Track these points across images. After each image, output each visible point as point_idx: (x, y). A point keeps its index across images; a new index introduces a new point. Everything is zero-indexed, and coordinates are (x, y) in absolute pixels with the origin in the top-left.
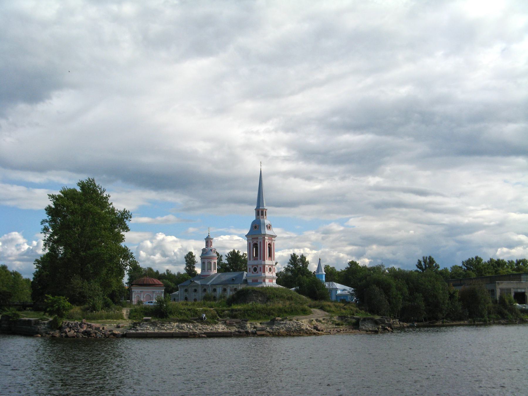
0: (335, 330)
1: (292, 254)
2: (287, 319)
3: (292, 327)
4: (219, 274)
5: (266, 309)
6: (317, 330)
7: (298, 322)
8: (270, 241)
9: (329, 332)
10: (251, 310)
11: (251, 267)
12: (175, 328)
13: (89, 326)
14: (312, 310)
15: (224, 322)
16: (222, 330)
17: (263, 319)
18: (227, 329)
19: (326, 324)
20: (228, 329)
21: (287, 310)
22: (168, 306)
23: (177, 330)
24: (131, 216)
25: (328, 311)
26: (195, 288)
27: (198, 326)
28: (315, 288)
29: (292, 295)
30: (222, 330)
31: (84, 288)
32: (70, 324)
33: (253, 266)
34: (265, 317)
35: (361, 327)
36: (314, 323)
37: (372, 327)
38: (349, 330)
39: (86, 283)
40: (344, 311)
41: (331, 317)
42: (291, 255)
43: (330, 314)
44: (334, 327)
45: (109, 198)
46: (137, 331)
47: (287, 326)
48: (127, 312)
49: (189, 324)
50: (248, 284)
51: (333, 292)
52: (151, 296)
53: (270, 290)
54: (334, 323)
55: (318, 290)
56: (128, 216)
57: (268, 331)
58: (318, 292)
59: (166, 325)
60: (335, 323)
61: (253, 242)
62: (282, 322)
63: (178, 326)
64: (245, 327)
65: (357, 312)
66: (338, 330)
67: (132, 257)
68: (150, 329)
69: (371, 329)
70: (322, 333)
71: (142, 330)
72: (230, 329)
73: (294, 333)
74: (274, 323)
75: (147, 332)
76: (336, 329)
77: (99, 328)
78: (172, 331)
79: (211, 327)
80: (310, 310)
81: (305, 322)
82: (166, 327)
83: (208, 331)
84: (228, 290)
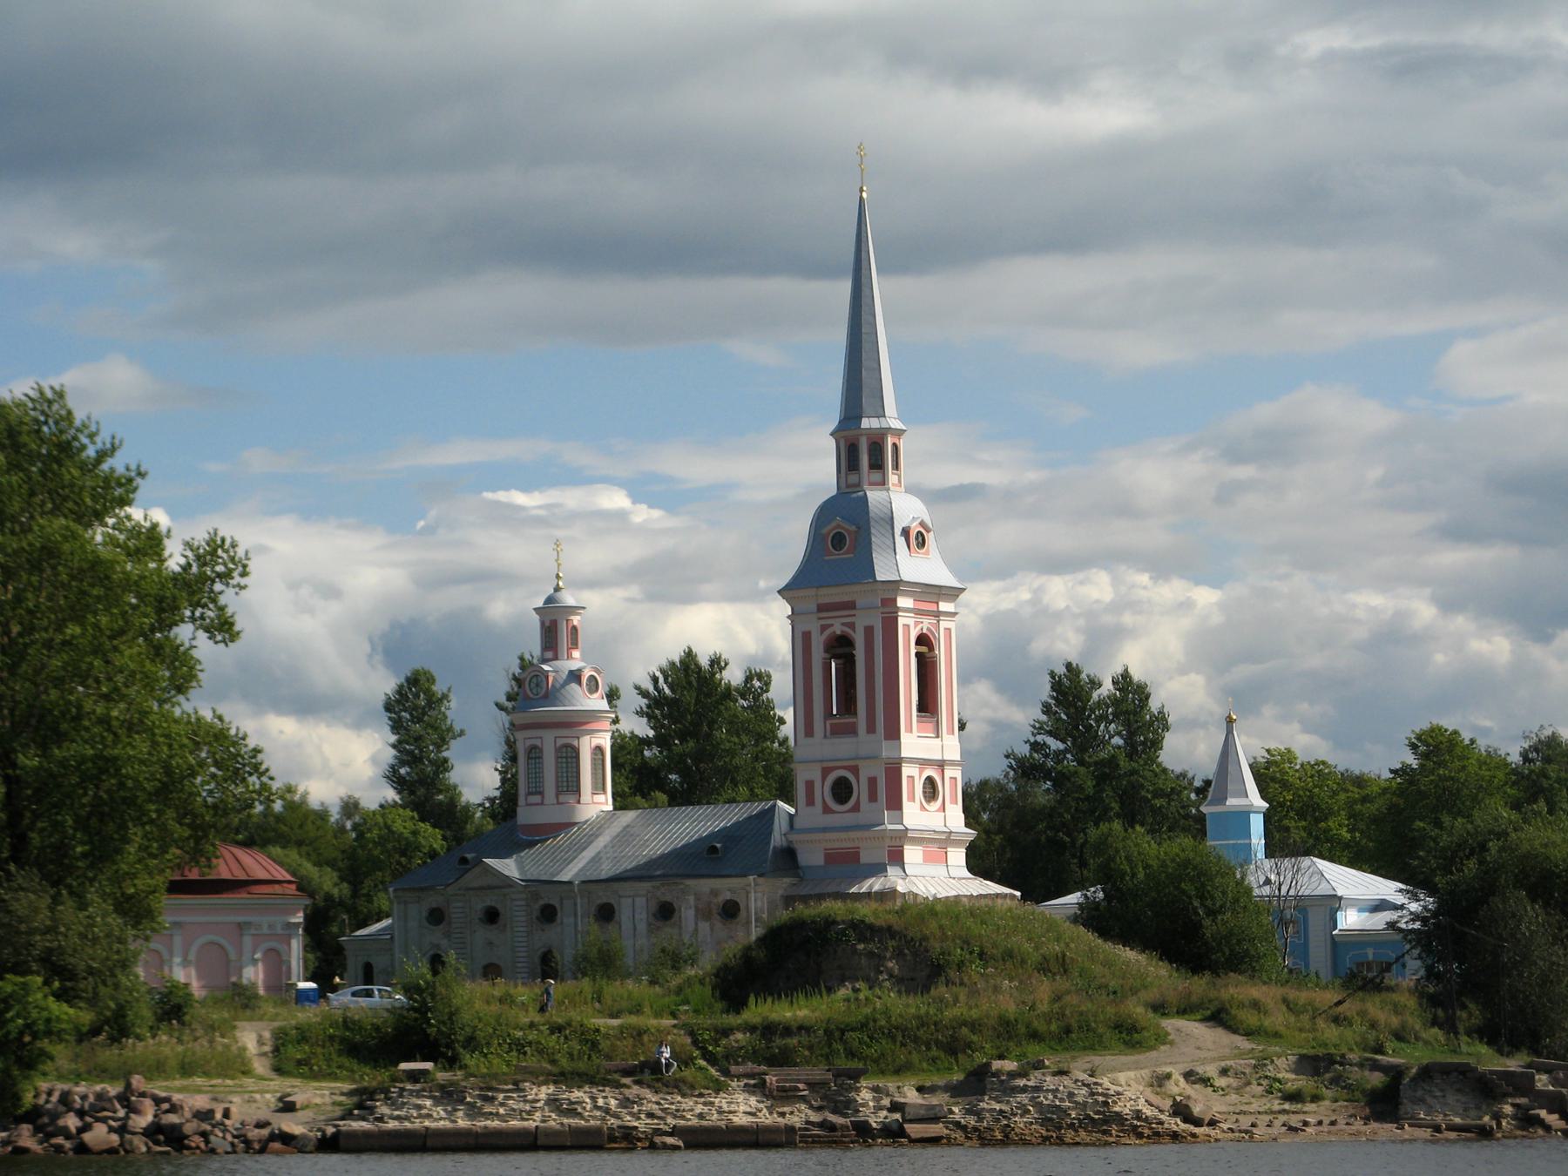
0: (1276, 1122)
1: (1061, 670)
2: (1044, 1067)
3: (1067, 1104)
4: (629, 816)
5: (935, 1024)
6: (1189, 1118)
7: (1096, 1084)
8: (926, 624)
9: (1246, 1132)
10: (863, 1026)
11: (815, 775)
12: (542, 1109)
13: (166, 1106)
14: (1170, 1024)
15: (752, 1082)
16: (751, 1119)
17: (923, 1071)
18: (771, 1113)
19: (1234, 1096)
20: (775, 1116)
21: (1039, 1025)
22: (458, 1010)
23: (555, 1121)
24: (245, 566)
25: (1249, 1034)
26: (490, 901)
27: (640, 1100)
28: (1196, 903)
29: (1067, 945)
30: (751, 1119)
31: (62, 929)
32: (77, 1098)
33: (826, 772)
34: (934, 1060)
35: (1409, 1109)
36: (1175, 1090)
37: (1466, 1110)
38: (1347, 1124)
39: (67, 908)
40: (1331, 1033)
41: (1262, 1062)
42: (1052, 674)
43: (1259, 1044)
44: (1276, 1107)
45: (139, 480)
46: (381, 1124)
47: (1047, 1099)
48: (261, 1042)
49: (604, 1091)
50: (802, 879)
51: (1316, 921)
52: (227, 955)
53: (945, 922)
54: (1272, 1087)
55: (1212, 913)
56: (231, 566)
57: (958, 1124)
58: (1209, 928)
59: (501, 1096)
60: (1280, 1090)
61: (823, 628)
62: (1021, 1082)
63: (553, 1102)
64: (852, 1107)
65: (1399, 1036)
66: (1295, 1121)
67: (256, 769)
68: (435, 1114)
69: (1458, 1120)
70: (1214, 1133)
71: (398, 1118)
72: (783, 1115)
73: (1076, 1131)
74: (985, 1087)
75: (427, 1128)
76: (1283, 1118)
77: (211, 1112)
78: (531, 1124)
79: (700, 1106)
80: (1158, 1026)
81: (1132, 1083)
82: (502, 1105)
83: (690, 1123)
84: (687, 914)
